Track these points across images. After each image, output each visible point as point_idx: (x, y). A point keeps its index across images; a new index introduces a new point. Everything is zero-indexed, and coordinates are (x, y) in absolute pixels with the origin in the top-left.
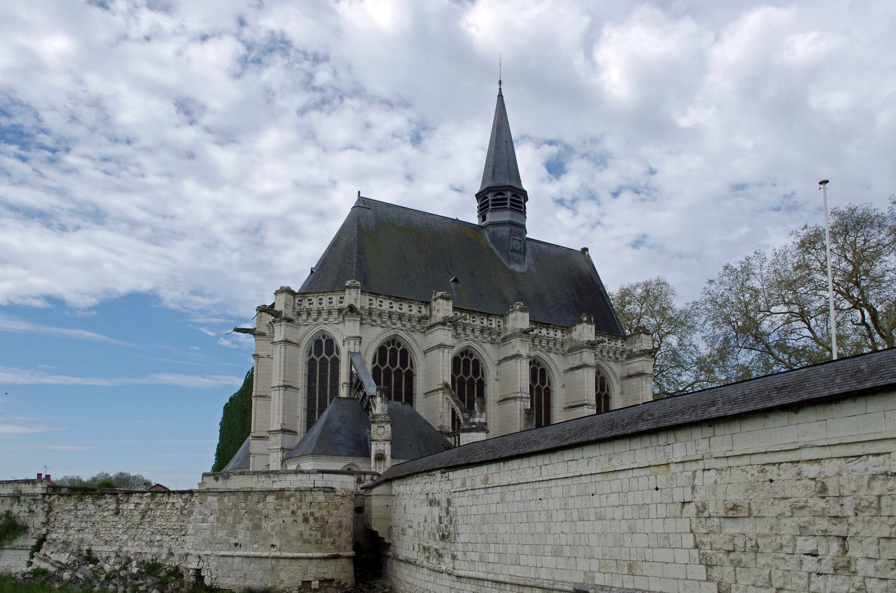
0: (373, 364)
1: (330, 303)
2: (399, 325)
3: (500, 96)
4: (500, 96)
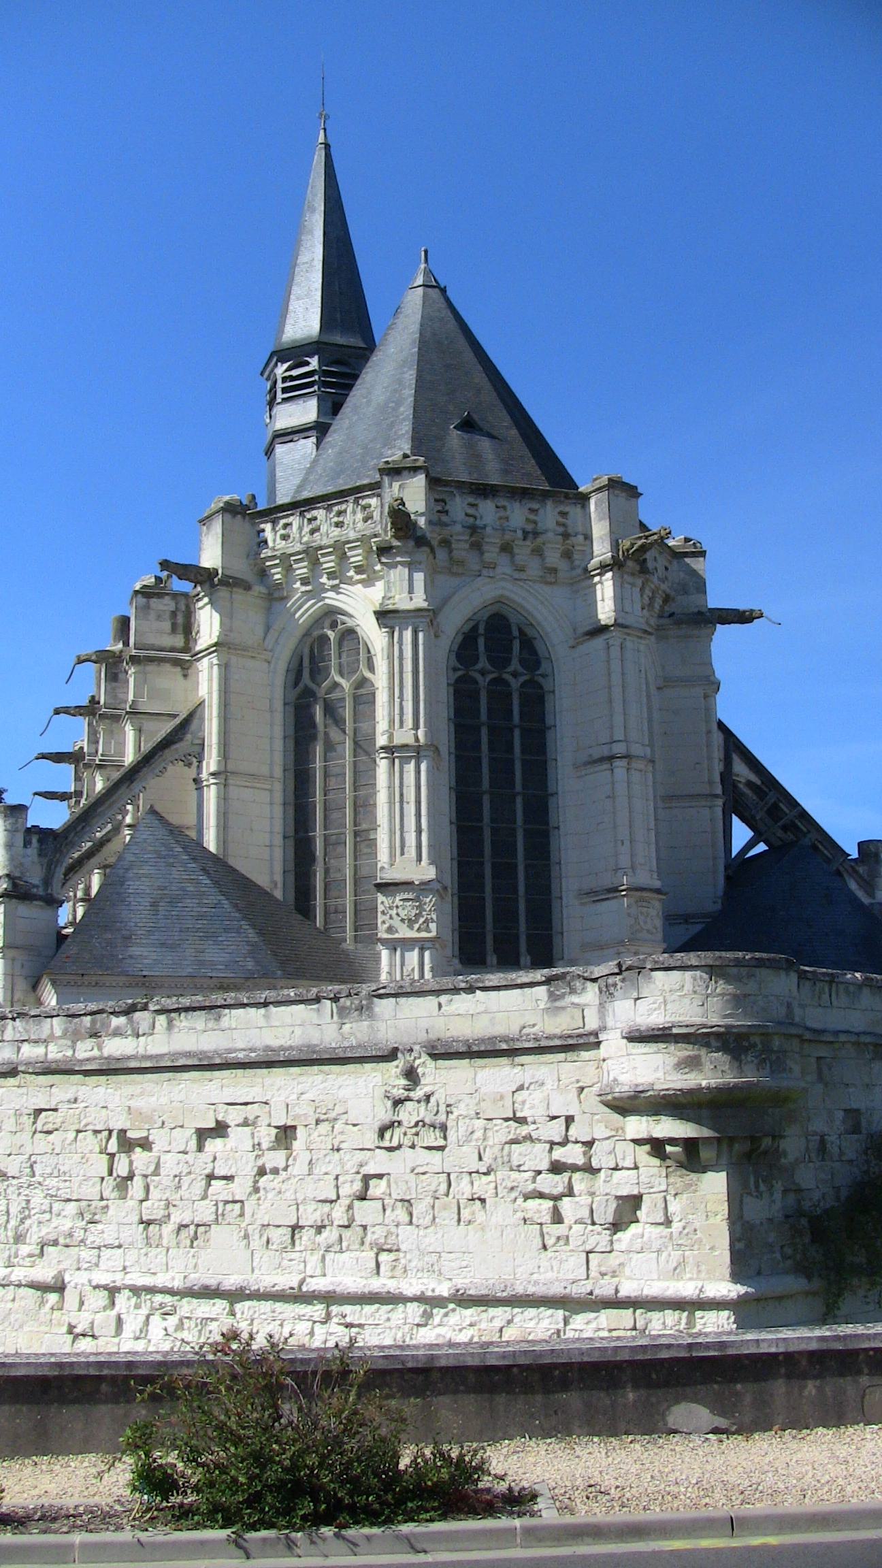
0: (296, 684)
1: (312, 532)
2: (504, 567)
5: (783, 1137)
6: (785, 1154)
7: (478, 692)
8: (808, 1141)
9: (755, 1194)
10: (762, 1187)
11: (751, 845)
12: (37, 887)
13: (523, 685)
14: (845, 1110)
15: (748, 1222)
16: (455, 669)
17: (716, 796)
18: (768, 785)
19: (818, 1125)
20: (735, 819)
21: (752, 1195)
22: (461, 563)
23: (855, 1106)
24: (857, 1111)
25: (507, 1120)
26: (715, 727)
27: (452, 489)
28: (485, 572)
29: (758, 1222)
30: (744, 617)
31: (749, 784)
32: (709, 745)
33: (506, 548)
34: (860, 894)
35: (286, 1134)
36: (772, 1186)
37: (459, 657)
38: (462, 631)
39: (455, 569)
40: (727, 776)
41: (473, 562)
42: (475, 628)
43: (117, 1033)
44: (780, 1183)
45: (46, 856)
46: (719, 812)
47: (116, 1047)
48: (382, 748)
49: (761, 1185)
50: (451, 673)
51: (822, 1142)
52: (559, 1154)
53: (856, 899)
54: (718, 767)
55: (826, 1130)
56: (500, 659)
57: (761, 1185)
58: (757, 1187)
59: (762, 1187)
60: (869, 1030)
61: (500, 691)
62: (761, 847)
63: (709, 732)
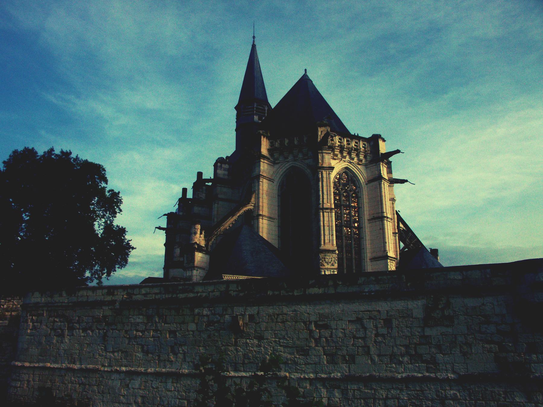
2: (348, 158)
3: (254, 47)
4: (254, 47)
12: (203, 247)
17: (397, 233)
22: (337, 155)
28: (343, 159)
30: (403, 181)
39: (335, 157)
43: (313, 286)
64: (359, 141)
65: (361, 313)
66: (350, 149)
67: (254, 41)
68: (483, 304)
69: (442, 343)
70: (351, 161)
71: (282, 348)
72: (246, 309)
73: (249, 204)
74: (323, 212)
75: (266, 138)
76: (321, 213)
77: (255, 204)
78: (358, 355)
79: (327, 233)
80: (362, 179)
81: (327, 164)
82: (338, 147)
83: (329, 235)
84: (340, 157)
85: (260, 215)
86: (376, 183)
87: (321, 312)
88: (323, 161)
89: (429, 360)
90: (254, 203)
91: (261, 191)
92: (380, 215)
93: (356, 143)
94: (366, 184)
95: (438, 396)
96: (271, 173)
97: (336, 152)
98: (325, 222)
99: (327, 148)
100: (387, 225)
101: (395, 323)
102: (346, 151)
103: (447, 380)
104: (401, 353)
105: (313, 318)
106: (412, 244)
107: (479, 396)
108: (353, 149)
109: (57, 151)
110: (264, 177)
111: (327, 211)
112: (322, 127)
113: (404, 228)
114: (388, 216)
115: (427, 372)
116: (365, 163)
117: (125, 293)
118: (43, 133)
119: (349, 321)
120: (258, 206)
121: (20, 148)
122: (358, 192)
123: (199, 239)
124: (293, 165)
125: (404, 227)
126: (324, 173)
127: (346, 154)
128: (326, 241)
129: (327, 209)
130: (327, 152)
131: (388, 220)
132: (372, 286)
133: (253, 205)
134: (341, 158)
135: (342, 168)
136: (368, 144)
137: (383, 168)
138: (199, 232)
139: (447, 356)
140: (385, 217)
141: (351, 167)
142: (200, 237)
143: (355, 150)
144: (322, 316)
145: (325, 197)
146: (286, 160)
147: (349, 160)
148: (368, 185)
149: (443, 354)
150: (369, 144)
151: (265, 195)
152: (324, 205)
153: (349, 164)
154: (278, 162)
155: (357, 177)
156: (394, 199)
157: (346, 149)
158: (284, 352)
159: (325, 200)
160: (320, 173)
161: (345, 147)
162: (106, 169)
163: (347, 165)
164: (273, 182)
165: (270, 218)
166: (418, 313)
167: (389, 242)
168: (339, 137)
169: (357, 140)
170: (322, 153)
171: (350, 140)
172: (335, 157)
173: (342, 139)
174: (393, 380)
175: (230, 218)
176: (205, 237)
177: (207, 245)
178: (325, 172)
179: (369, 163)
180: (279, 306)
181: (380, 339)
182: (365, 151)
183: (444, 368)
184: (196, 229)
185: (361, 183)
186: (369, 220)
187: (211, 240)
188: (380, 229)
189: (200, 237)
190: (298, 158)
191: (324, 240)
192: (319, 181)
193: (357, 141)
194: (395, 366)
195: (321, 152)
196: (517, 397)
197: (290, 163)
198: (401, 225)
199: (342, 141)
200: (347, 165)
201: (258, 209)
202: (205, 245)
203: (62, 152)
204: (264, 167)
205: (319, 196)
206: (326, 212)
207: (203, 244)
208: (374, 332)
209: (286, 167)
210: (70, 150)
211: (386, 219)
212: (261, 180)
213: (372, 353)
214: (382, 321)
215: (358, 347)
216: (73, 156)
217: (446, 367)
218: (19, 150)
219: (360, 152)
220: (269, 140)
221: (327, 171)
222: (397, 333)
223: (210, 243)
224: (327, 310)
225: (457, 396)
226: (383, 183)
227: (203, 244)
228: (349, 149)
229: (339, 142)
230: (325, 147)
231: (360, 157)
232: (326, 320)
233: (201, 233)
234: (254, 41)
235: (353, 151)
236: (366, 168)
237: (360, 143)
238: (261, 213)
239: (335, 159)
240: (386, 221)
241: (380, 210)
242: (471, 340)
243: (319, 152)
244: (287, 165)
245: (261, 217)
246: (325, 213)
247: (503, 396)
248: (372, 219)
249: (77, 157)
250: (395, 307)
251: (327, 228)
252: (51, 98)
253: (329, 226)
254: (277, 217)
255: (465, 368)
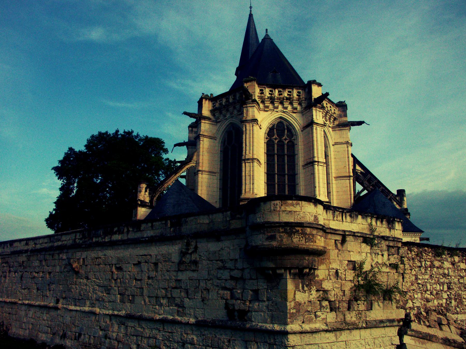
2: (280, 107)
3: (251, 16)
4: (251, 16)
5: (317, 269)
6: (318, 276)
7: (274, 145)
8: (329, 272)
9: (302, 291)
10: (306, 288)
11: (362, 191)
12: (148, 203)
13: (288, 143)
14: (348, 261)
15: (298, 302)
16: (267, 138)
17: (351, 176)
18: (367, 172)
19: (335, 266)
20: (357, 183)
21: (300, 291)
22: (268, 107)
23: (352, 259)
24: (355, 261)
25: (217, 261)
26: (350, 156)
27: (265, 86)
28: (275, 110)
29: (303, 302)
30: (360, 123)
31: (361, 173)
32: (348, 161)
33: (282, 103)
34: (397, 207)
35: (156, 264)
36: (311, 288)
37: (268, 135)
38: (270, 127)
39: (266, 109)
40: (354, 170)
41: (271, 107)
42: (274, 126)
44: (315, 287)
45: (151, 194)
46: (352, 181)
47: (116, 237)
48: (367, 222)
49: (305, 287)
50: (265, 139)
51: (337, 273)
52: (233, 273)
53: (396, 208)
54: (351, 168)
55: (338, 268)
56: (281, 135)
57: (305, 287)
58: (303, 288)
59: (306, 288)
60: (360, 231)
61: (281, 145)
62: (366, 192)
63: (348, 157)
64: (293, 90)
65: (140, 257)
66: (281, 99)
67: (251, 11)
68: (222, 249)
69: (189, 287)
70: (285, 110)
71: (97, 287)
72: (82, 254)
73: (191, 161)
74: (245, 163)
75: (209, 101)
76: (244, 164)
77: (197, 161)
78: (137, 295)
79: (248, 182)
80: (297, 127)
81: (251, 117)
82: (268, 99)
83: (250, 184)
84: (273, 109)
85: (200, 171)
86: (309, 129)
87: (118, 256)
88: (247, 115)
89: (179, 303)
90: (196, 160)
91: (201, 150)
92: (311, 160)
93: (289, 92)
94: (302, 131)
95: (181, 339)
96: (214, 131)
97: (266, 104)
98: (247, 172)
99: (251, 102)
100: (318, 170)
101: (160, 266)
102: (277, 102)
103: (187, 324)
104: (162, 296)
105: (114, 262)
106: (371, 185)
107: (209, 343)
108: (285, 98)
109: (121, 132)
110: (204, 136)
111: (249, 161)
112: (248, 82)
113: (362, 171)
114: (320, 161)
115: (178, 315)
116: (300, 110)
117: (33, 243)
118: (170, 114)
119: (134, 264)
120: (199, 163)
121: (96, 133)
122: (294, 140)
123: (144, 196)
124: (232, 121)
125: (362, 169)
126: (247, 125)
127: (277, 105)
128: (247, 190)
129: (248, 159)
130: (251, 105)
131: (319, 164)
132: (149, 232)
133: (195, 162)
134: (273, 109)
135: (275, 119)
136: (303, 91)
137: (316, 114)
138: (144, 190)
139: (191, 300)
140: (316, 161)
141: (285, 116)
142: (145, 194)
143: (287, 99)
144: (119, 260)
145: (248, 148)
146: (225, 118)
147: (282, 109)
148: (304, 131)
149: (189, 299)
150: (305, 90)
151: (206, 153)
152: (246, 156)
153: (283, 114)
154: (219, 120)
155: (292, 124)
156: (348, 142)
157: (277, 99)
158: (99, 291)
159: (247, 151)
160: (244, 126)
161: (276, 97)
162: (164, 141)
163: (281, 114)
164: (216, 140)
165: (211, 173)
166: (175, 258)
167: (319, 187)
168: (270, 89)
169: (290, 89)
170: (247, 107)
171: (281, 90)
172: (266, 109)
173: (273, 91)
174: (151, 320)
175: (174, 175)
176: (149, 194)
177: (151, 201)
178: (249, 125)
179: (304, 109)
180: (97, 251)
181: (150, 281)
182: (299, 99)
183: (188, 312)
184: (141, 188)
185: (297, 131)
186: (303, 166)
187: (155, 196)
188: (312, 174)
189: (145, 194)
190: (233, 115)
191: (245, 189)
192: (242, 134)
193: (290, 90)
194: (158, 308)
195: (245, 106)
196: (238, 346)
197: (229, 120)
198: (358, 168)
199: (274, 92)
200: (281, 114)
201: (199, 166)
202: (150, 201)
203: (125, 132)
204: (205, 127)
205: (242, 148)
206: (247, 162)
207: (147, 200)
208: (147, 275)
209: (226, 125)
210: (132, 130)
211: (317, 164)
212: (201, 139)
213: (144, 294)
214: (152, 265)
215: (137, 288)
216: (135, 134)
217: (190, 311)
218: (95, 135)
219: (293, 100)
220: (212, 102)
221: (250, 123)
222: (160, 277)
223: (155, 199)
224: (121, 255)
225: (194, 341)
226: (315, 128)
227: (147, 200)
228: (280, 100)
229: (269, 94)
230: (248, 101)
231: (294, 106)
232: (121, 263)
233: (146, 191)
234: (251, 11)
235: (284, 101)
236: (303, 115)
237: (293, 92)
238: (200, 169)
239: (267, 111)
240: (316, 165)
241: (312, 154)
242: (210, 285)
243: (244, 106)
244: (227, 123)
245: (201, 173)
246: (247, 164)
247: (226, 344)
248: (305, 165)
249: (137, 134)
250: (161, 251)
251: (248, 178)
252: (174, 85)
253: (250, 176)
254: (219, 171)
255: (203, 314)
